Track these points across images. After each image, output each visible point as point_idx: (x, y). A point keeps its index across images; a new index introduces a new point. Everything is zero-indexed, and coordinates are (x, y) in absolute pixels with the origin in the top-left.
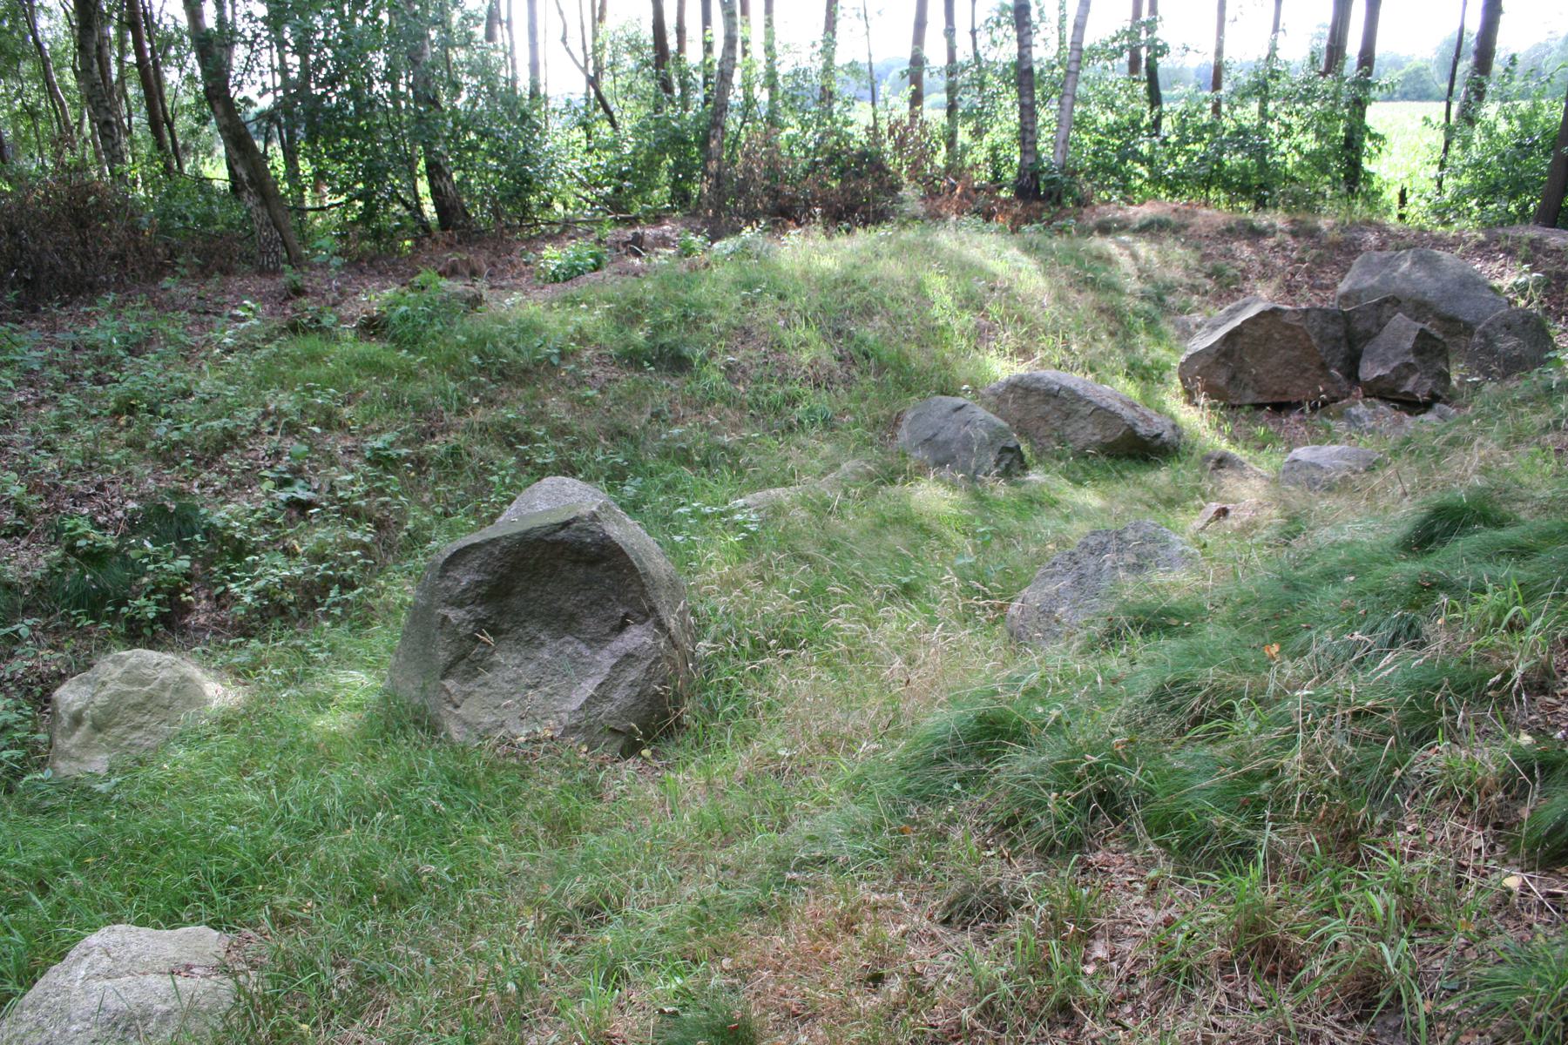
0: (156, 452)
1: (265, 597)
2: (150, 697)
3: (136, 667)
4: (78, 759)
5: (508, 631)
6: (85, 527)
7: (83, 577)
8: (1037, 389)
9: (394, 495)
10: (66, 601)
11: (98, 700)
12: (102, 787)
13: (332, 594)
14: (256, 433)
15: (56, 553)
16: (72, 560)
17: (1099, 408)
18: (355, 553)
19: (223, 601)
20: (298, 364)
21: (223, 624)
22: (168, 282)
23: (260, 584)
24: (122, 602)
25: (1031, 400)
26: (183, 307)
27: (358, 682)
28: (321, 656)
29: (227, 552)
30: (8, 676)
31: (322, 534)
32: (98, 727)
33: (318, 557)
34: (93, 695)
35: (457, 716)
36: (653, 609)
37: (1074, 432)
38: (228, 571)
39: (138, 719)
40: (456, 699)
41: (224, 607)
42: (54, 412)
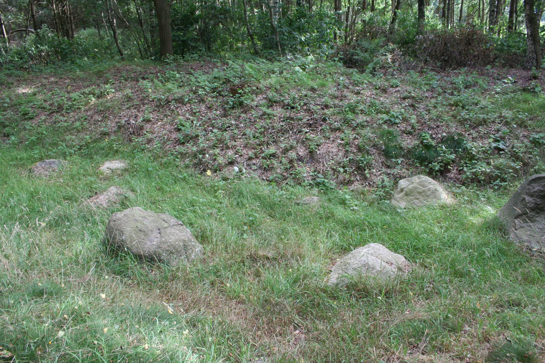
0: (460, 121)
1: (474, 175)
2: (424, 191)
3: (424, 181)
4: (398, 201)
6: (428, 137)
7: (422, 152)
9: (535, 156)
10: (415, 157)
11: (410, 187)
12: (399, 210)
13: (497, 181)
14: (494, 122)
15: (417, 142)
16: (421, 146)
18: (510, 171)
19: (461, 172)
20: (519, 102)
21: (458, 179)
22: (489, 67)
23: (474, 170)
24: (430, 163)
26: (491, 76)
27: (490, 211)
28: (483, 199)
29: (468, 157)
30: (392, 173)
31: (501, 161)
32: (407, 195)
33: (497, 168)
34: (409, 185)
35: (515, 233)
38: (466, 163)
39: (418, 197)
40: (517, 227)
41: (460, 174)
42: (435, 101)
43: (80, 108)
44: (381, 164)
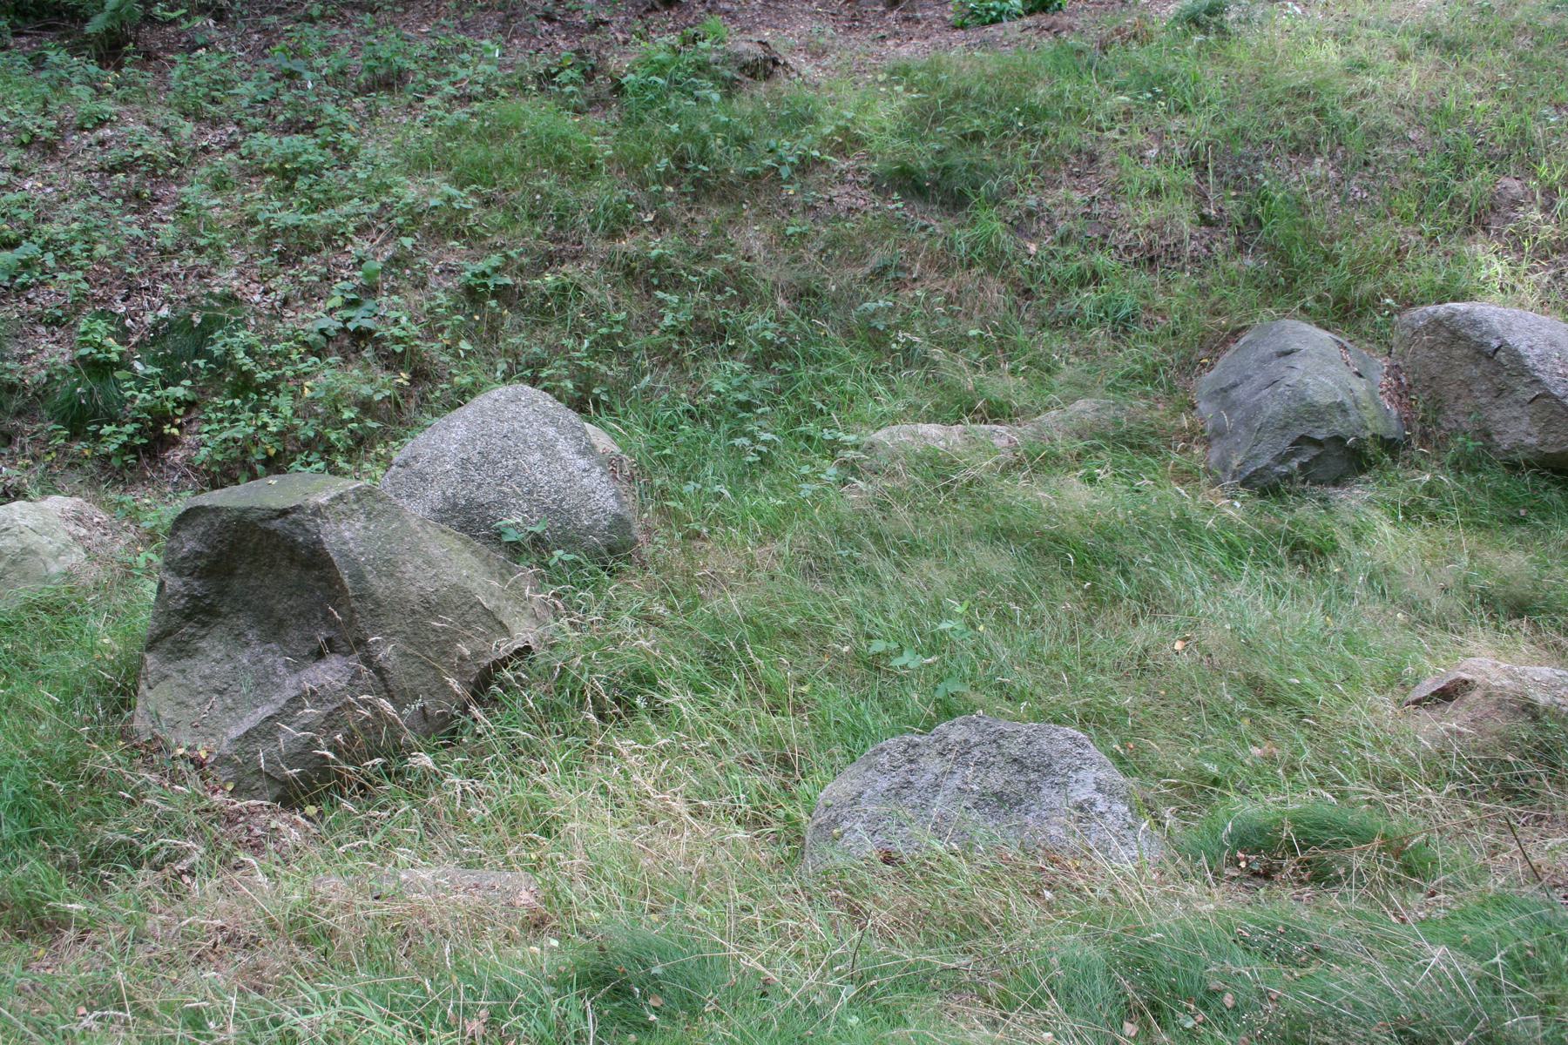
8: (1467, 338)
17: (1548, 395)
25: (1457, 352)
32: (942, 388)
37: (1506, 421)
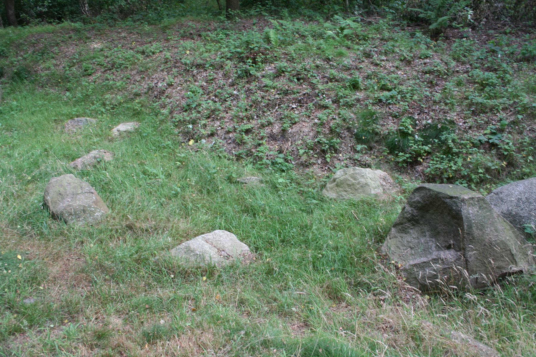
2: (353, 184)
5: (421, 225)
32: (337, 186)
36: (464, 249)
43: (127, 67)
44: (350, 148)
